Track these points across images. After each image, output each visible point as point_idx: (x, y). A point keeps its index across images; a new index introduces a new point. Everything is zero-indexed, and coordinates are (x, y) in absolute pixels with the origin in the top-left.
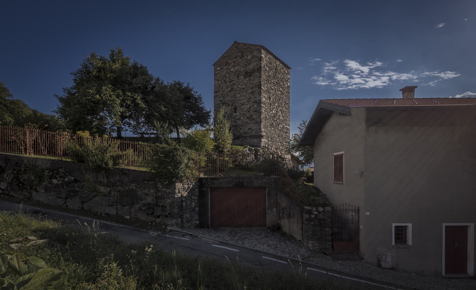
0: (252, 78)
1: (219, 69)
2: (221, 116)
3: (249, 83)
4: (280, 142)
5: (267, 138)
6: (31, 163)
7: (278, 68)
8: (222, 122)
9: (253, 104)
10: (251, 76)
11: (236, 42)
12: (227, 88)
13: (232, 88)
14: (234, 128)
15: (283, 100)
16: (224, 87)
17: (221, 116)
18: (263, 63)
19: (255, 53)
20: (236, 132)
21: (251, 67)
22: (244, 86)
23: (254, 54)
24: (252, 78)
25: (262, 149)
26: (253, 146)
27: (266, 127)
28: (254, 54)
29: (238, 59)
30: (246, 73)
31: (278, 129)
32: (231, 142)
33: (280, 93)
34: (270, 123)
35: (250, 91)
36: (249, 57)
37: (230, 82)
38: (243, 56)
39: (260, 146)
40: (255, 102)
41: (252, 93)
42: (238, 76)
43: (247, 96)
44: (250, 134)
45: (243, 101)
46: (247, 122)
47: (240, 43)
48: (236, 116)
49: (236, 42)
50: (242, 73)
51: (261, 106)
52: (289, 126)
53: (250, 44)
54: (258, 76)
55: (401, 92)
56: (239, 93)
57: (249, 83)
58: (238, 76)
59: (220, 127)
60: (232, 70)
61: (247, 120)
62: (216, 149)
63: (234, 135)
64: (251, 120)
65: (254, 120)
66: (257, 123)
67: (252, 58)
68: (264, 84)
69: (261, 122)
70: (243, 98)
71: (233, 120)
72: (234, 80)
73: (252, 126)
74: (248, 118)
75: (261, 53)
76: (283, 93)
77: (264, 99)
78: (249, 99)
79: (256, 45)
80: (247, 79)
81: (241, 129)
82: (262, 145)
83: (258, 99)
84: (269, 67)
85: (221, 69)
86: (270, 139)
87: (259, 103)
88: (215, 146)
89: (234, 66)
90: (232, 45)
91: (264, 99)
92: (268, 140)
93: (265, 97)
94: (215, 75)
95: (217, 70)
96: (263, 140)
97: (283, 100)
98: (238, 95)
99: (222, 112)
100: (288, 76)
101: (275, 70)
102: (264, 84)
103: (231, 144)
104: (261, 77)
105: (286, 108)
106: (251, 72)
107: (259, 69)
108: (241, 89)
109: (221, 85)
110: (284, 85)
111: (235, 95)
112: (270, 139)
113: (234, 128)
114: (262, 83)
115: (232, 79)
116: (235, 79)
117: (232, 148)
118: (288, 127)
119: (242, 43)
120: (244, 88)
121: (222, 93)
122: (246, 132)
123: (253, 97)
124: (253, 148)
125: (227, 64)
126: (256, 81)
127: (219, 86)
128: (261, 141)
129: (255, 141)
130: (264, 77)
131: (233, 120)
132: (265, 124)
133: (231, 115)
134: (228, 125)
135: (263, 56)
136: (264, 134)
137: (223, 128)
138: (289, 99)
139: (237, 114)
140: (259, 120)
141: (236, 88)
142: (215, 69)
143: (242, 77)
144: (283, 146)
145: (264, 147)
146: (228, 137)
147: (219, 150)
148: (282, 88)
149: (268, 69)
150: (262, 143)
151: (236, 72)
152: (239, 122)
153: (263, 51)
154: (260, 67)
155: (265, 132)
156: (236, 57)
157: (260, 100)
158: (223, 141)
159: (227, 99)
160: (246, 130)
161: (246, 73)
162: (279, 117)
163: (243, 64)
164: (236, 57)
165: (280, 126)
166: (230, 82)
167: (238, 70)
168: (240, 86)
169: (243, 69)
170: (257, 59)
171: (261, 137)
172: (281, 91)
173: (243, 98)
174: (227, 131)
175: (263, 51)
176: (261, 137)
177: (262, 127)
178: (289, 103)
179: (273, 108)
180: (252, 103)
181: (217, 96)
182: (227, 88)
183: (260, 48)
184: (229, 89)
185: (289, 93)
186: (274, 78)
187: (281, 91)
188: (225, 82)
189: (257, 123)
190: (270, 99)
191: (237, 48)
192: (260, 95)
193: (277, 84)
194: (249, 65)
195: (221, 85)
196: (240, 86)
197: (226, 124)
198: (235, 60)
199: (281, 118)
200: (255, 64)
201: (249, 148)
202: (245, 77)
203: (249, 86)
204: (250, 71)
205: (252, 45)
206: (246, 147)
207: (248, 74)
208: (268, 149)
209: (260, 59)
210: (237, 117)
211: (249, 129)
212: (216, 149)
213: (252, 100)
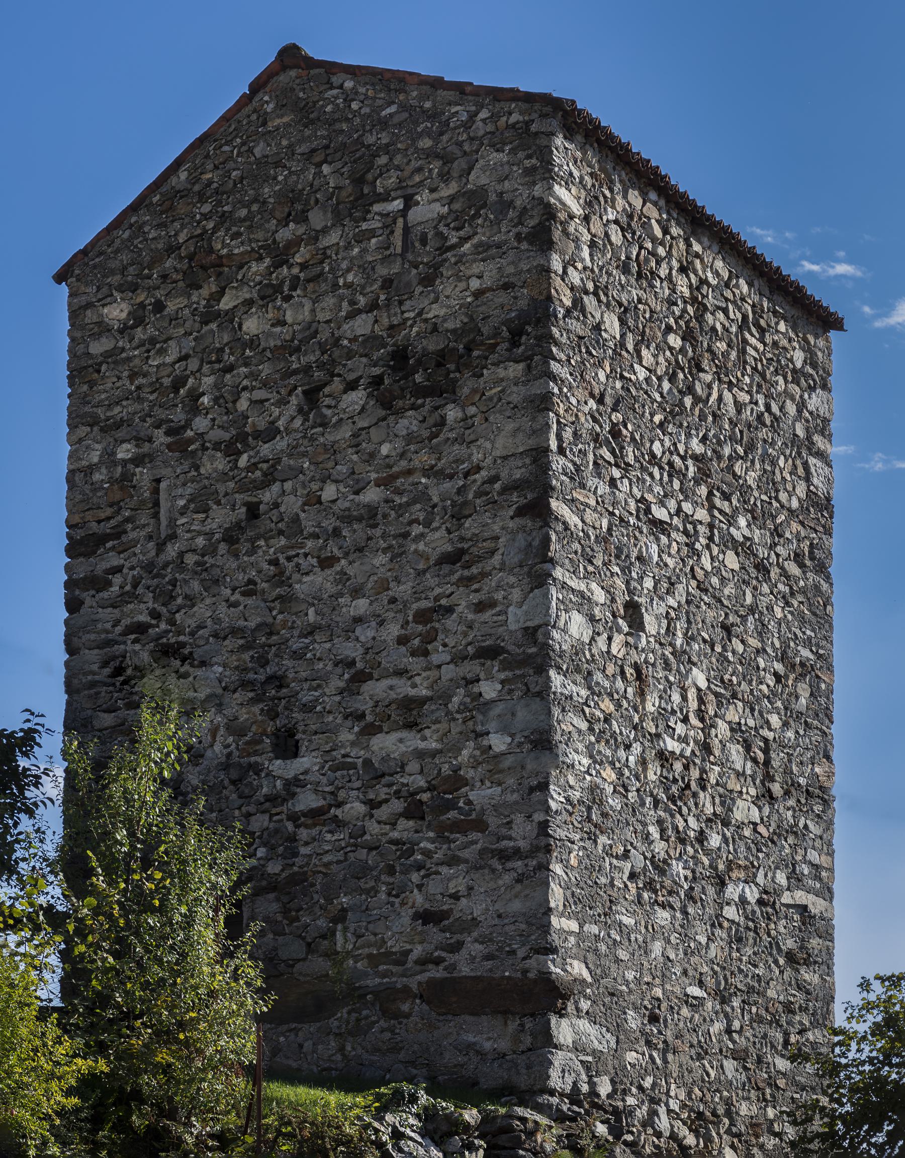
0: (452, 413)
1: (117, 312)
2: (140, 786)
3: (424, 458)
4: (740, 1056)
5: (608, 1014)
6: (189, 433)
7: (716, 320)
8: (152, 842)
9: (470, 668)
10: (443, 390)
11: (290, 56)
12: (201, 503)
13: (253, 512)
14: (270, 905)
15: (762, 631)
16: (175, 497)
17: (146, 790)
18: (570, 272)
19: (490, 169)
20: (293, 949)
21: (445, 305)
22: (372, 495)
23: (478, 178)
24: (452, 413)
25: (560, 1117)
26: (466, 1090)
27: (593, 901)
28: (478, 178)
29: (317, 219)
30: (400, 358)
31: (717, 921)
32: (246, 1045)
33: (732, 561)
34: (638, 860)
35: (438, 541)
36: (427, 209)
37: (231, 450)
38: (359, 201)
39: (532, 1092)
40: (489, 653)
41: (452, 558)
42: (312, 395)
43: (403, 590)
44: (437, 973)
45: (365, 633)
46: (406, 848)
47: (332, 68)
48: (294, 784)
49: (290, 56)
50: (359, 367)
51: (543, 693)
52: (827, 893)
53: (436, 83)
54: (516, 395)
55: (64, 289)
56: (326, 563)
57: (424, 458)
58: (312, 395)
59: (140, 902)
60: (252, 325)
61: (405, 828)
62: (97, 1121)
63: (275, 972)
64: (443, 833)
65: (480, 825)
66: (504, 856)
67: (458, 220)
68: (576, 476)
69: (542, 846)
70: (361, 606)
71: (260, 822)
72: (270, 433)
73: (458, 884)
74: (414, 811)
75: (544, 171)
76: (762, 568)
77: (577, 626)
78: (423, 617)
79: (497, 95)
80: (408, 423)
81: (341, 917)
82: (555, 1080)
83: (516, 619)
84: (625, 313)
85: (138, 318)
86: (633, 1021)
87: (530, 657)
88: (87, 1085)
89: (270, 294)
90: (257, 87)
91: (577, 626)
92: (618, 1029)
93: (584, 601)
94: (82, 371)
95: (103, 329)
96: (564, 1030)
97: (762, 631)
98: (313, 582)
99: (161, 739)
100: (814, 401)
101: (688, 336)
102: (576, 476)
103: (253, 1073)
104: (544, 403)
105: (790, 716)
106: (441, 358)
107: (529, 329)
108: (347, 518)
109: (143, 475)
110: (769, 482)
111: (280, 578)
112: (633, 1021)
113: (275, 906)
114: (558, 463)
115: (258, 421)
116: (286, 415)
117: (254, 1109)
118: (816, 905)
119: (352, 71)
120: (370, 515)
121: (145, 551)
122: (395, 945)
123: (463, 601)
124: (471, 1115)
125: (204, 265)
126: (497, 445)
127: (125, 481)
128: (547, 1040)
129: (489, 1035)
130: (574, 405)
131: (260, 822)
132: (592, 868)
133: (239, 773)
134: (210, 875)
135: (567, 198)
136: (578, 969)
137: (162, 910)
138: (823, 621)
139: (305, 762)
140: (522, 833)
141: (292, 504)
142: (75, 314)
143: (357, 397)
144: (765, 1089)
145: (574, 1096)
146: (224, 1000)
147: (123, 1125)
148: (756, 517)
149: (612, 325)
150: (559, 1058)
151: (290, 348)
152: (321, 847)
153: (564, 152)
154: (541, 312)
155: (589, 951)
156: (295, 206)
157: (537, 635)
158: (164, 1036)
159: (202, 611)
160: (398, 931)
161: (400, 358)
162: (727, 800)
163: (367, 269)
164: (295, 206)
165: (732, 891)
166: (231, 450)
167: (311, 329)
168: (329, 492)
169: (362, 326)
170: (506, 233)
171: (552, 996)
172: (744, 548)
173: (361, 606)
174: (207, 937)
175: (564, 152)
176: (552, 996)
177: (556, 896)
178: (825, 660)
179: (663, 714)
180: (458, 658)
181: (98, 583)
182: (201, 503)
183: (540, 120)
184: (221, 517)
185: (822, 568)
186: (675, 412)
187: (744, 548)
188: (180, 447)
189: (504, 856)
190: (637, 625)
191: (306, 114)
192: (539, 579)
193: (704, 474)
194: (428, 281)
195: (143, 475)
196: (329, 492)
197: (200, 872)
198: (285, 234)
199: (745, 810)
200: (483, 274)
201: (429, 1116)
202: (387, 403)
203: (422, 496)
204: (433, 345)
205: (461, 89)
206: (396, 1102)
207: (417, 376)
208: (618, 1120)
209: (542, 229)
210: (307, 800)
211: (427, 917)
212: (97, 1121)
213: (453, 633)
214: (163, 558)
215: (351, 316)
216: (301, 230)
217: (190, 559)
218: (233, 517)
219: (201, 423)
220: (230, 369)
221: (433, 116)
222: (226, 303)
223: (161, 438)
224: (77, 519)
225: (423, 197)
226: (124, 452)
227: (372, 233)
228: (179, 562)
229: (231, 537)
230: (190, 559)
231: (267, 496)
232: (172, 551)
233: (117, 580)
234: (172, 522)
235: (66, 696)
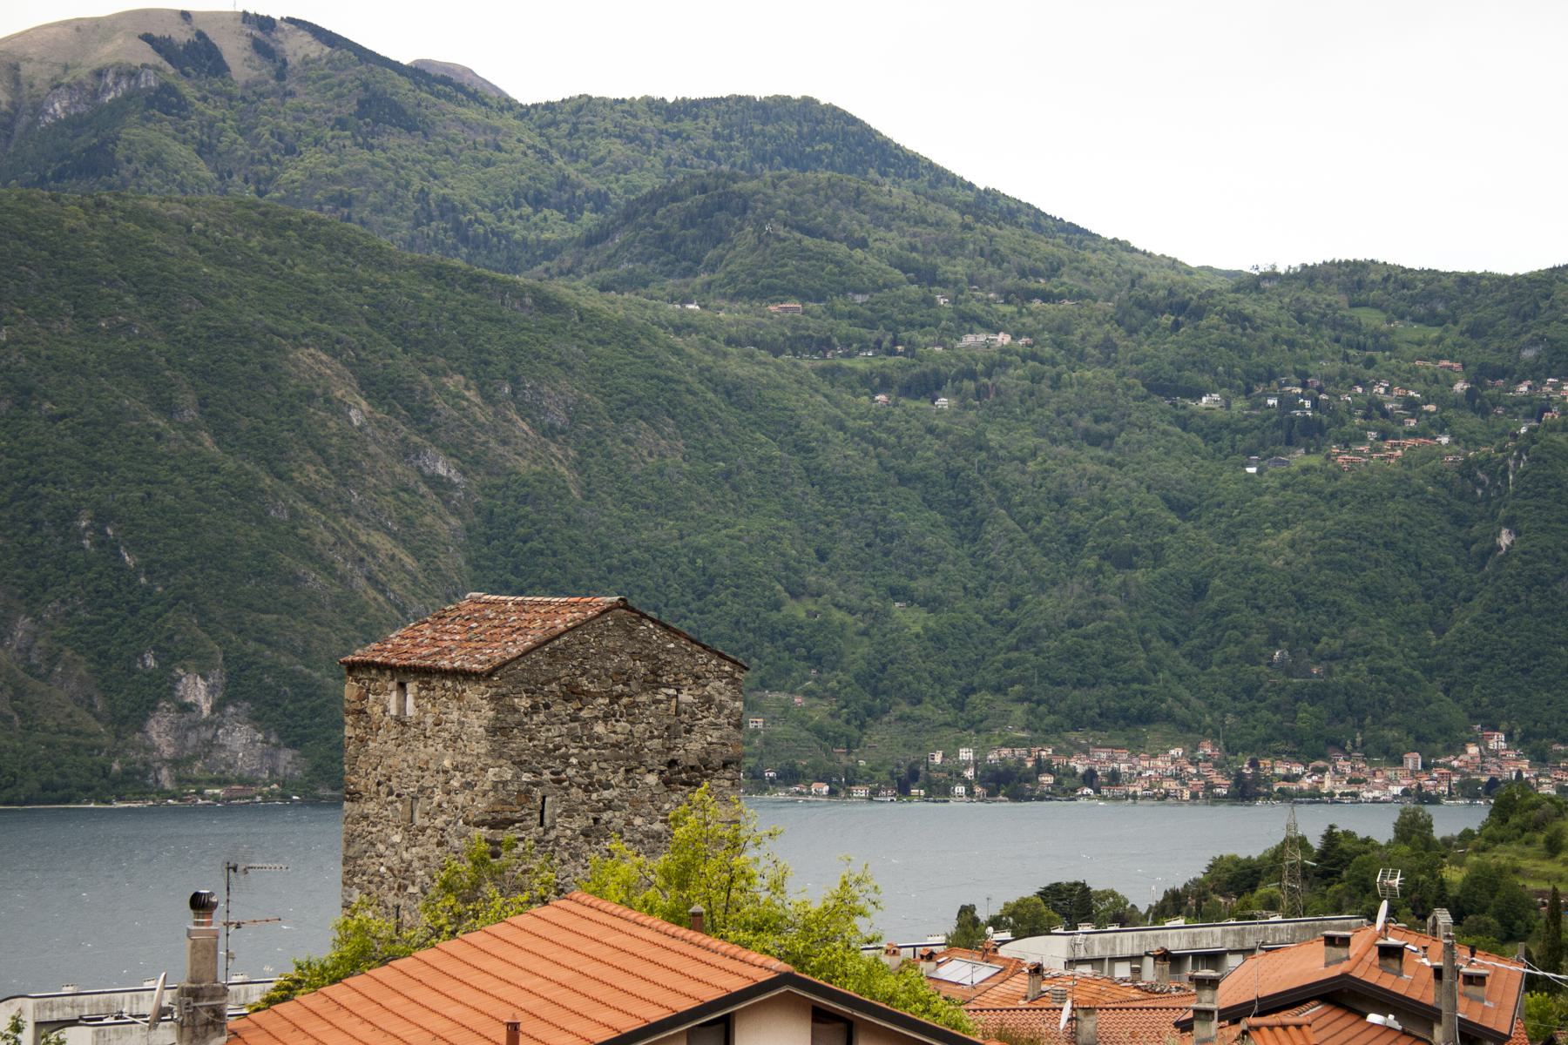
10: (693, 784)
22: (657, 826)
60: (599, 728)
85: (535, 708)
168: (638, 821)
182: (569, 813)
184: (579, 823)
195: (537, 793)
196: (638, 821)
214: (547, 838)
215: (651, 738)
216: (627, 690)
217: (563, 842)
218: (585, 824)
219: (571, 772)
220: (586, 748)
221: (691, 655)
222: (584, 714)
223: (547, 775)
224: (1001, 203)
225: (685, 691)
226: (526, 777)
227: (660, 702)
228: (557, 840)
229: (586, 834)
230: (563, 842)
231: (606, 816)
232: (553, 834)
233: (521, 845)
234: (553, 821)
235: (670, 100)
